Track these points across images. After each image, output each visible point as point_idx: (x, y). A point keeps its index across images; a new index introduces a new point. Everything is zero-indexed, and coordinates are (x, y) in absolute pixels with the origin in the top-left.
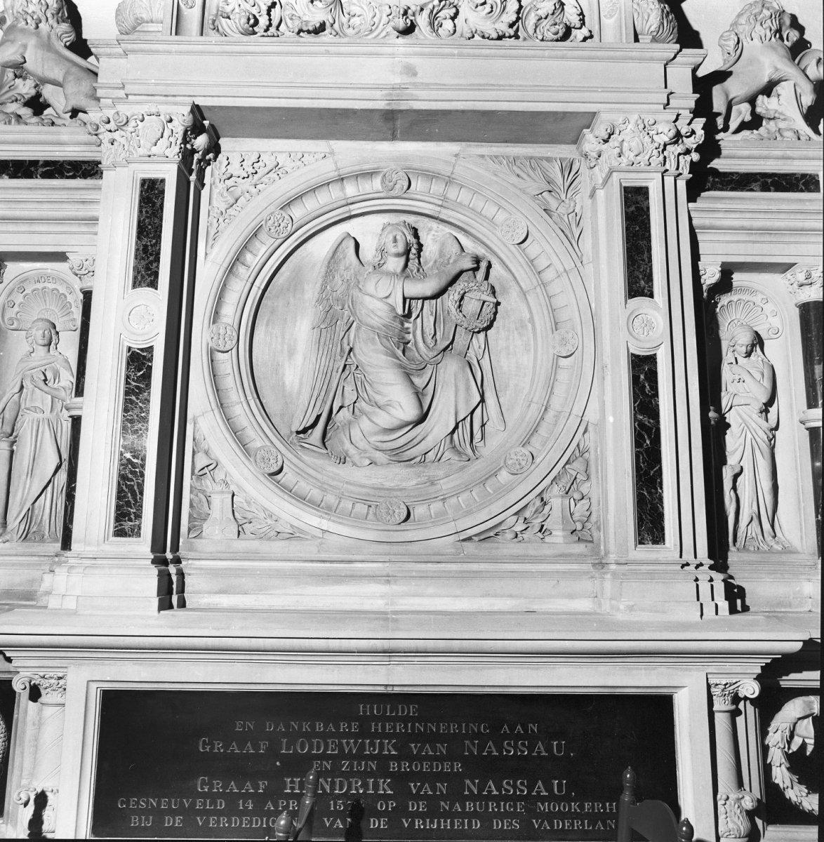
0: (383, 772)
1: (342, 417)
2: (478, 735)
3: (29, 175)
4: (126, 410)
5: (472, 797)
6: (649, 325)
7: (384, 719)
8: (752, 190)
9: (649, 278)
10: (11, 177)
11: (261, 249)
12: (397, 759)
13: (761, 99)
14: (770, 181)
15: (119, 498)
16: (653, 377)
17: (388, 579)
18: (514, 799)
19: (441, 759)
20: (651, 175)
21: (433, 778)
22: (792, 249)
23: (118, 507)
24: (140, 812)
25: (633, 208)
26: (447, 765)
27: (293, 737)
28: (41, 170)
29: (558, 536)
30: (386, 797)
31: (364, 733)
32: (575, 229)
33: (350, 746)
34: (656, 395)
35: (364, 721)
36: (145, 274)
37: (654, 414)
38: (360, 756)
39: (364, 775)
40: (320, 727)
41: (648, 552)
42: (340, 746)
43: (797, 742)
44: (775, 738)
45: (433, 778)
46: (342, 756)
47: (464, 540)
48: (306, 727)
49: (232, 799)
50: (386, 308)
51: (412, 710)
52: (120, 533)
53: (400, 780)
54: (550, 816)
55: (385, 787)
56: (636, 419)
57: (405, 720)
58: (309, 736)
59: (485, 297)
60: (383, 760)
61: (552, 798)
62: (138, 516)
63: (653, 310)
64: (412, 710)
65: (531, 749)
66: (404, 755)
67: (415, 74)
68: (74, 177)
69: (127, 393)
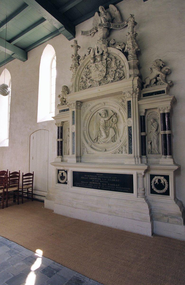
0: (99, 182)
1: (99, 138)
3: (65, 111)
5: (109, 186)
6: (130, 122)
7: (99, 176)
8: (153, 95)
9: (131, 115)
10: (63, 112)
11: (88, 116)
12: (101, 180)
13: (158, 78)
14: (156, 93)
16: (131, 129)
18: (114, 186)
19: (105, 181)
21: (105, 183)
25: (129, 104)
26: (106, 182)
30: (100, 185)
31: (97, 177)
32: (71, 125)
33: (96, 179)
34: (132, 132)
35: (97, 176)
36: (73, 123)
37: (131, 135)
38: (97, 180)
39: (98, 182)
40: (93, 176)
42: (95, 179)
43: (156, 183)
44: (153, 182)
45: (105, 183)
47: (112, 153)
49: (85, 184)
53: (101, 183)
54: (118, 189)
55: (100, 184)
56: (129, 136)
58: (92, 177)
59: (116, 119)
60: (99, 181)
62: (75, 152)
63: (131, 120)
64: (101, 175)
65: (116, 180)
66: (101, 180)
67: (100, 91)
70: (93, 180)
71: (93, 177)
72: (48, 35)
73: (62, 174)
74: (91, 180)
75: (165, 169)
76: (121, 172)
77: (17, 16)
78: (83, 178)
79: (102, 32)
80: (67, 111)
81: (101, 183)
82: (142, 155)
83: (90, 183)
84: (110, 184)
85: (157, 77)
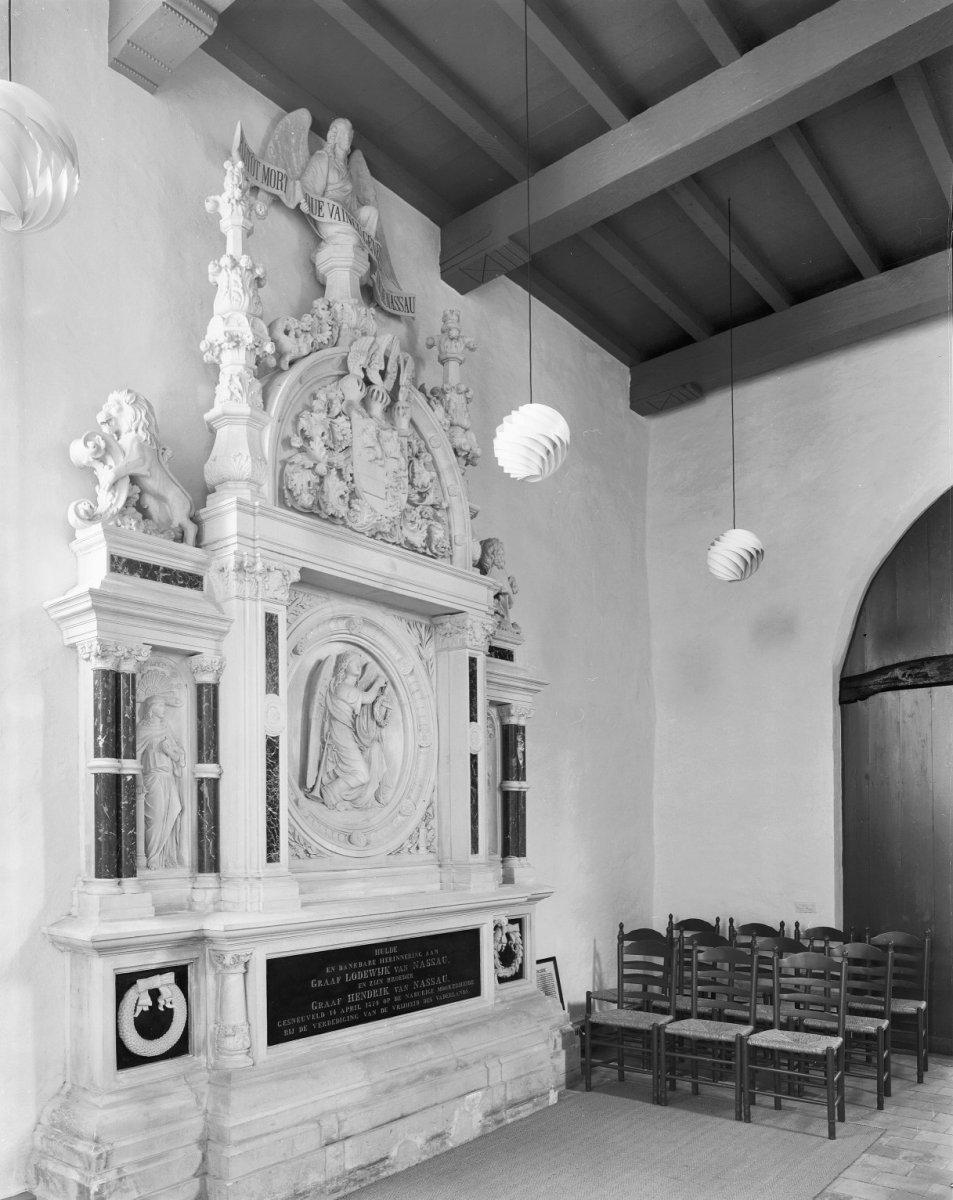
2: (417, 959)
3: (154, 578)
4: (268, 779)
15: (268, 838)
17: (364, 879)
20: (479, 653)
22: (506, 695)
23: (268, 844)
24: (288, 1027)
27: (350, 971)
28: (162, 575)
29: (423, 849)
35: (377, 958)
38: (376, 978)
40: (361, 965)
41: (473, 859)
46: (370, 978)
48: (361, 965)
49: (326, 1010)
50: (350, 710)
51: (394, 950)
52: (270, 860)
53: (391, 986)
57: (392, 955)
58: (356, 970)
61: (444, 985)
66: (393, 974)
67: (396, 569)
68: (183, 585)
69: (267, 767)
70: (362, 980)
71: (362, 969)
72: (863, 604)
73: (155, 994)
74: (352, 987)
75: (341, 925)
76: (299, 946)
77: (579, 66)
78: (320, 982)
79: (361, 269)
80: (166, 580)
81: (391, 986)
82: (201, 869)
83: (351, 997)
84: (419, 984)
85: (198, 509)
